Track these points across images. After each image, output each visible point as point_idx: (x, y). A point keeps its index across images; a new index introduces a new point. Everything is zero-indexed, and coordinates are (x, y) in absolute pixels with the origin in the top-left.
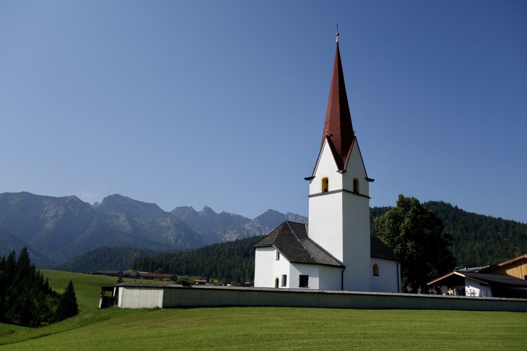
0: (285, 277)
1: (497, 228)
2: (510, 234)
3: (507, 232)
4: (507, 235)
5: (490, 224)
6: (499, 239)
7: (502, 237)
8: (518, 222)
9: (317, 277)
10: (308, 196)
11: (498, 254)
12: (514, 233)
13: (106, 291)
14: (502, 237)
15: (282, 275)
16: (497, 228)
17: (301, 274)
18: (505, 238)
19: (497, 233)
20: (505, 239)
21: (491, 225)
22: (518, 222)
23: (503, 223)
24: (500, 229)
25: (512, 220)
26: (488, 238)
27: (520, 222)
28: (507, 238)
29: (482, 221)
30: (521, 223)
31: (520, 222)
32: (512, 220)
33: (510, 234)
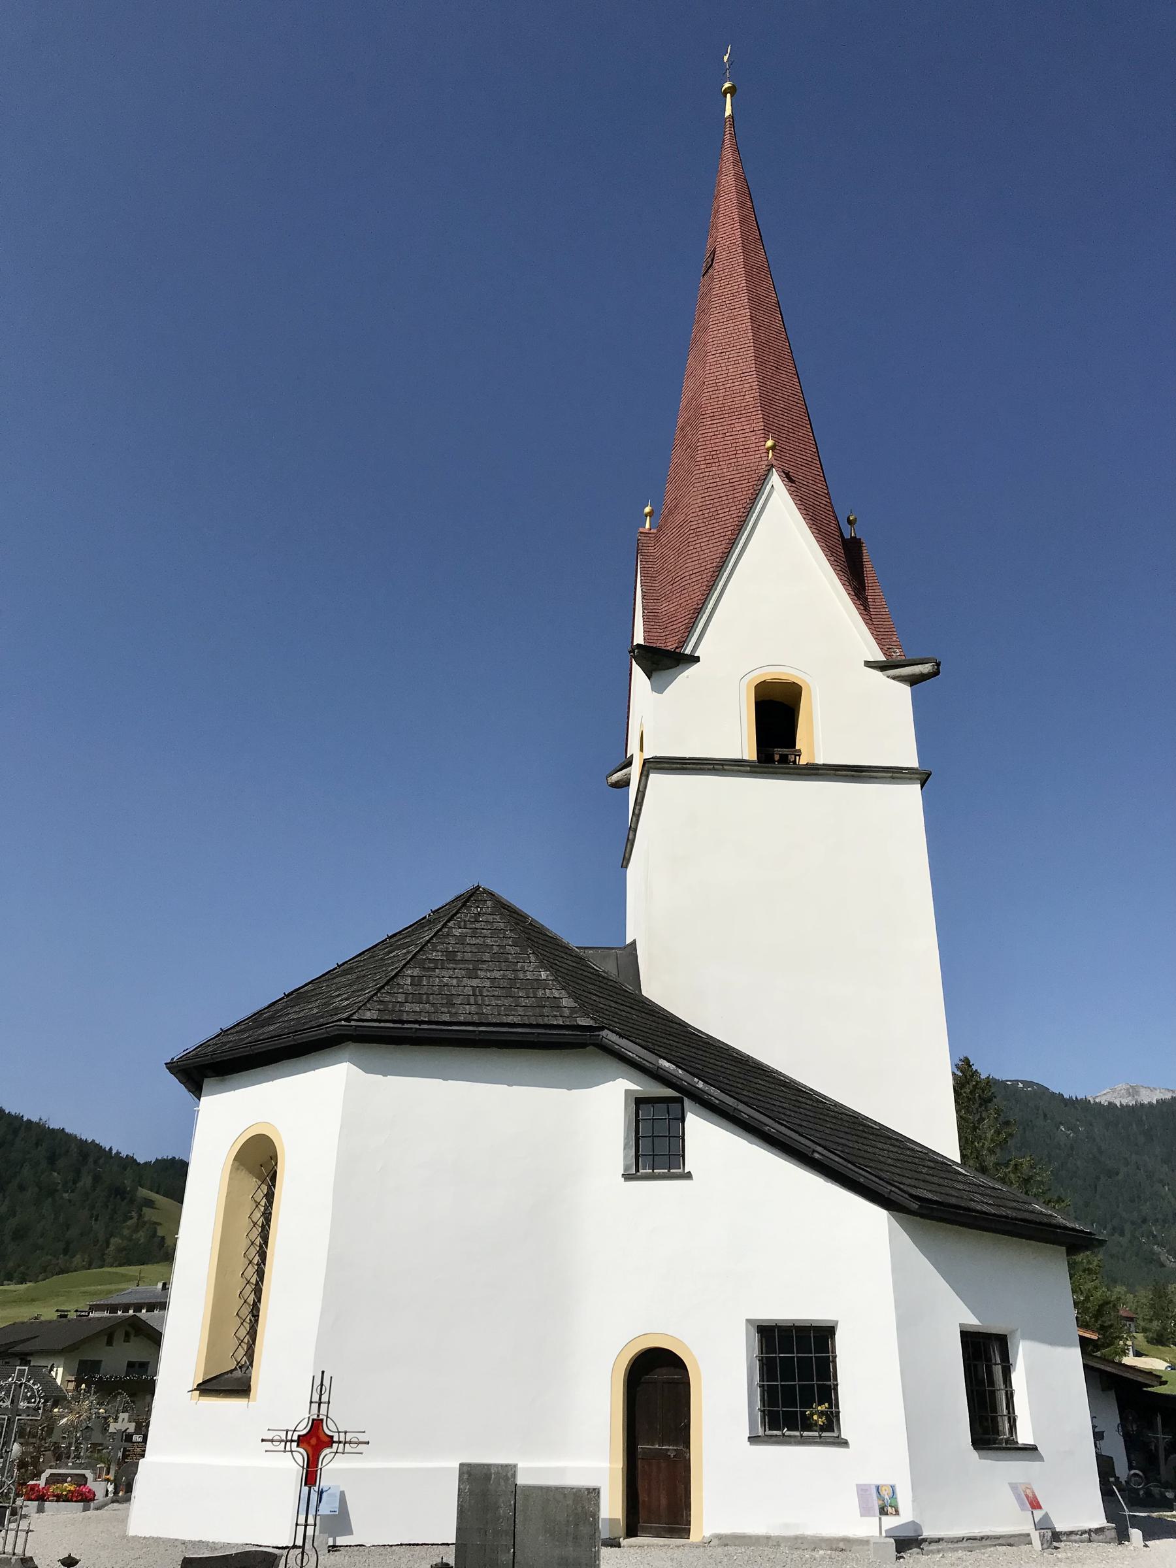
0: (57, 1311)
1: (52, 1159)
2: (86, 1181)
3: (78, 1173)
4: (75, 1182)
5: (37, 1145)
6: (52, 1192)
7: (60, 1187)
8: (107, 1149)
9: (1077, 1346)
10: (635, 940)
11: (41, 1241)
12: (97, 1179)
13: (337, 1538)
14: (60, 1187)
15: (748, 1321)
16: (52, 1159)
17: (972, 1321)
18: (67, 1192)
19: (51, 1174)
20: (66, 1195)
21: (39, 1148)
22: (107, 1149)
23: (73, 1145)
24: (61, 1163)
25: (93, 1141)
26: (22, 1188)
27: (111, 1149)
28: (72, 1191)
29: (16, 1132)
30: (114, 1152)
31: (111, 1149)
32: (93, 1141)
33: (86, 1181)
